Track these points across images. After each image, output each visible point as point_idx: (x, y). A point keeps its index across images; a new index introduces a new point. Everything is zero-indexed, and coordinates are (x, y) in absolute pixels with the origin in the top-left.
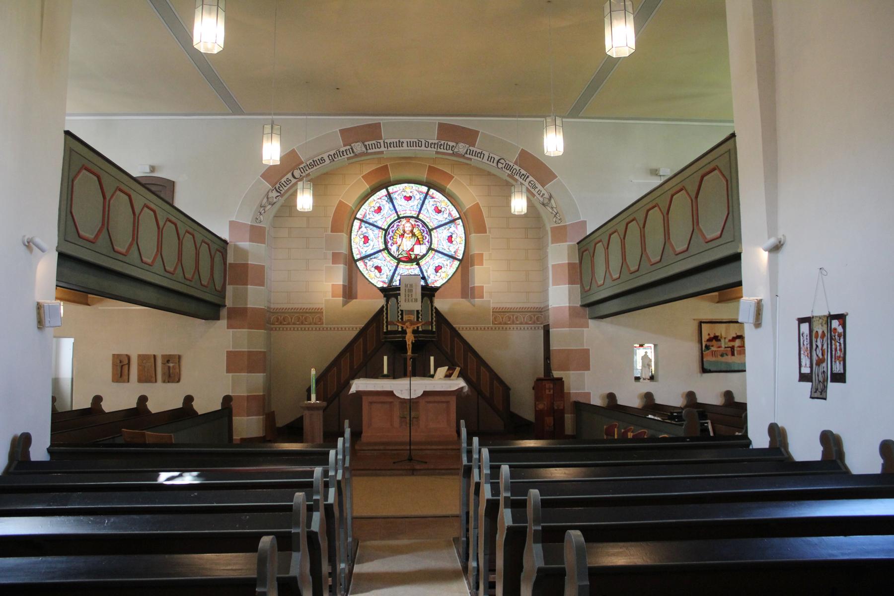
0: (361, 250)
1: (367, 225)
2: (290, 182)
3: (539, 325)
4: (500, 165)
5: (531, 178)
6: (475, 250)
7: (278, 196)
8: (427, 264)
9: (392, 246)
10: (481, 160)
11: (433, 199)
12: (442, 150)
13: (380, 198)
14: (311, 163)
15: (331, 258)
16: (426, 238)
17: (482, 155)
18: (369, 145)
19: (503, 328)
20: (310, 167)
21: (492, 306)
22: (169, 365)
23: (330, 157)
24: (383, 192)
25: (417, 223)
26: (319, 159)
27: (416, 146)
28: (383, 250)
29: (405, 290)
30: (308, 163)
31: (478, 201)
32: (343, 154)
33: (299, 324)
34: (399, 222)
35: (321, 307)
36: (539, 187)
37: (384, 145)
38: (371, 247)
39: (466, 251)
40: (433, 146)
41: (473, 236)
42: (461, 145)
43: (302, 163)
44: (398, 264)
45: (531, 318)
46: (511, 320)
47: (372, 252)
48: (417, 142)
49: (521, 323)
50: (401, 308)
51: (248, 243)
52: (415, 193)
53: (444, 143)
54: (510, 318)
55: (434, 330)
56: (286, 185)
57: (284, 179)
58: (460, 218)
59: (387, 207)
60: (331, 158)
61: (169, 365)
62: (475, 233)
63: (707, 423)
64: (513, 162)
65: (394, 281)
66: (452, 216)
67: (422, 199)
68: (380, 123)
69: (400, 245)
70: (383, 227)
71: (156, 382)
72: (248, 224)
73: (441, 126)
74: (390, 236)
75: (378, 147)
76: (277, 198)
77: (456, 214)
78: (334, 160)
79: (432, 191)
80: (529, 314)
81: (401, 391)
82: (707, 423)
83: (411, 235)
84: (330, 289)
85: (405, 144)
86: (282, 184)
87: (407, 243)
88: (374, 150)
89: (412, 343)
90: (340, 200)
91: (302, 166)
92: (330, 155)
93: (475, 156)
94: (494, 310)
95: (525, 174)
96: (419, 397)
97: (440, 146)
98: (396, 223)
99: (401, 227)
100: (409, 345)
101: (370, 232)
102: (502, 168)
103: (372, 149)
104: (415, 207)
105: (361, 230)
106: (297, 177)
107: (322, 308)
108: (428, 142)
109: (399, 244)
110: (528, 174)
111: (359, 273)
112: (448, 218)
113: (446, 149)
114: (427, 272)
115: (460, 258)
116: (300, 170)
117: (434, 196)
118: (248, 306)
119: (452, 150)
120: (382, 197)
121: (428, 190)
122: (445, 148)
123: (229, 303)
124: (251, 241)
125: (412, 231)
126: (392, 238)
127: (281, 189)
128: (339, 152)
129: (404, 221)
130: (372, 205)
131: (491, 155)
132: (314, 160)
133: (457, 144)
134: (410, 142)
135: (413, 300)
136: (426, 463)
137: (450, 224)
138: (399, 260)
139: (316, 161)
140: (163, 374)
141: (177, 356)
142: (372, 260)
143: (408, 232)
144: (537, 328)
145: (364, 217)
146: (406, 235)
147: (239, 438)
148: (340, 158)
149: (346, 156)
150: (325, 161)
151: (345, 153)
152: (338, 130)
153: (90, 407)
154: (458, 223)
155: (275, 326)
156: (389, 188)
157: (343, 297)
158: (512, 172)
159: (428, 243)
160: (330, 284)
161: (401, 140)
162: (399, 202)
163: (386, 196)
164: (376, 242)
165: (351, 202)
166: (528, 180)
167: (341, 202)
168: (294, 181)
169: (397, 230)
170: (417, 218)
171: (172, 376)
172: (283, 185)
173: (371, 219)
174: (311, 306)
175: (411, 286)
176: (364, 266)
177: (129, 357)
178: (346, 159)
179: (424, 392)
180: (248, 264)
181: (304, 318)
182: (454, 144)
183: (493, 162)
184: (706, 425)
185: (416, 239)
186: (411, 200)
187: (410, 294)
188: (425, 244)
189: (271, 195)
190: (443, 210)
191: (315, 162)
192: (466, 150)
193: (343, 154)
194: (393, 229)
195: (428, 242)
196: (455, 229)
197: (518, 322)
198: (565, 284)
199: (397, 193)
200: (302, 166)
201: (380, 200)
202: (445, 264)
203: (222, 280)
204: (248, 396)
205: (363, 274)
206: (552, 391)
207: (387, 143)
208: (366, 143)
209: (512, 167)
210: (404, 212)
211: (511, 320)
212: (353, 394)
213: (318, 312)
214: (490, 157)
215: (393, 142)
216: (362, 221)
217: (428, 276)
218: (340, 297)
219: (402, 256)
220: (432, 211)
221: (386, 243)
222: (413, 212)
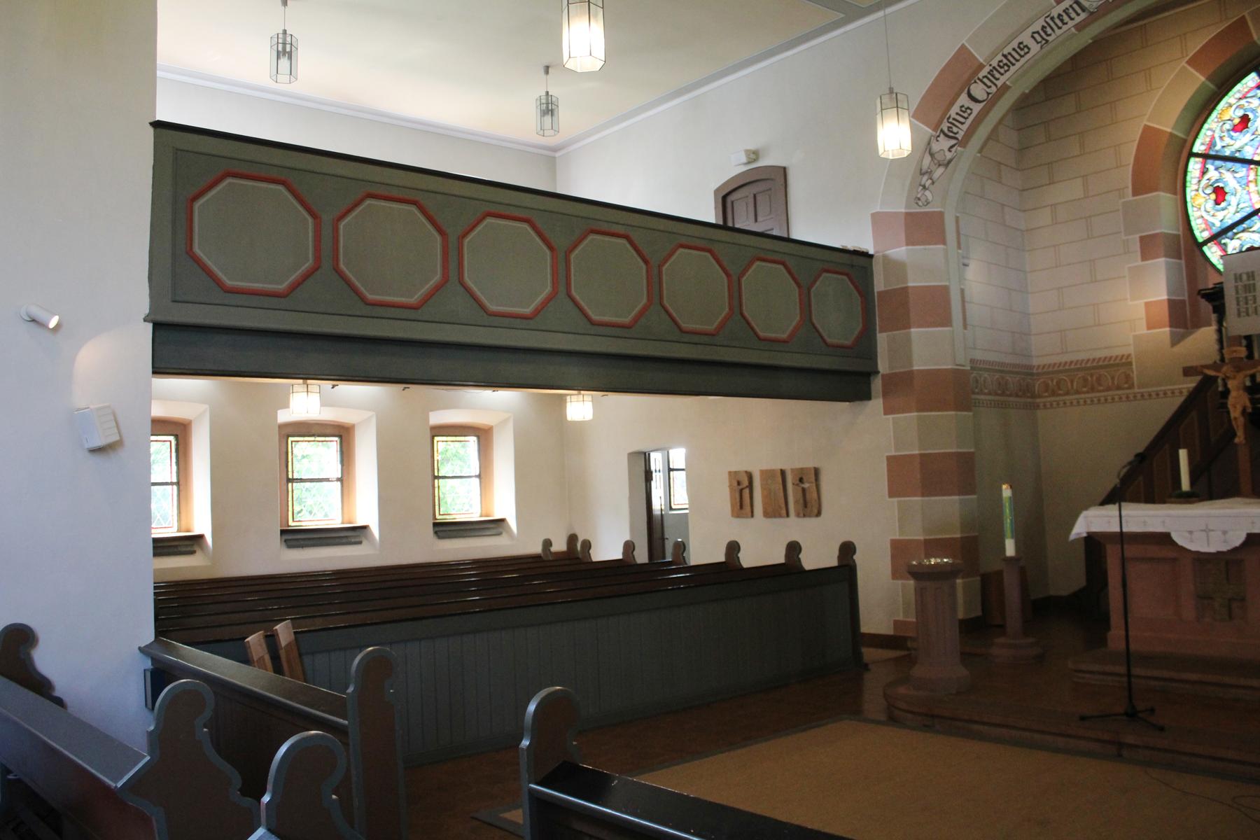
1: (1218, 163)
2: (969, 111)
14: (1001, 61)
15: (1139, 249)
20: (1002, 71)
22: (803, 485)
26: (1014, 49)
29: (1236, 287)
30: (995, 63)
32: (1062, 21)
33: (1088, 392)
35: (1126, 353)
38: (1232, 209)
43: (981, 67)
47: (1238, 217)
51: (904, 248)
56: (962, 120)
57: (955, 109)
60: (1039, 39)
61: (803, 485)
71: (788, 515)
72: (902, 212)
76: (953, 149)
78: (1047, 41)
81: (1191, 532)
84: (1141, 313)
86: (954, 119)
89: (1244, 412)
92: (1034, 33)
101: (1228, 176)
105: (1206, 177)
106: (980, 99)
107: (1129, 356)
116: (981, 81)
120: (1248, 92)
123: (883, 366)
124: (909, 242)
127: (955, 130)
128: (1052, 19)
132: (1005, 52)
136: (1162, 729)
139: (1010, 54)
145: (1210, 148)
148: (1058, 32)
149: (1071, 23)
150: (1029, 49)
151: (1066, 18)
153: (620, 557)
160: (1141, 303)
168: (977, 108)
171: (810, 506)
173: (1226, 149)
177: (750, 476)
178: (1073, 29)
181: (1055, 381)
187: (1250, 296)
189: (936, 147)
193: (1062, 21)
201: (1243, 102)
212: (1073, 541)
218: (1164, 327)
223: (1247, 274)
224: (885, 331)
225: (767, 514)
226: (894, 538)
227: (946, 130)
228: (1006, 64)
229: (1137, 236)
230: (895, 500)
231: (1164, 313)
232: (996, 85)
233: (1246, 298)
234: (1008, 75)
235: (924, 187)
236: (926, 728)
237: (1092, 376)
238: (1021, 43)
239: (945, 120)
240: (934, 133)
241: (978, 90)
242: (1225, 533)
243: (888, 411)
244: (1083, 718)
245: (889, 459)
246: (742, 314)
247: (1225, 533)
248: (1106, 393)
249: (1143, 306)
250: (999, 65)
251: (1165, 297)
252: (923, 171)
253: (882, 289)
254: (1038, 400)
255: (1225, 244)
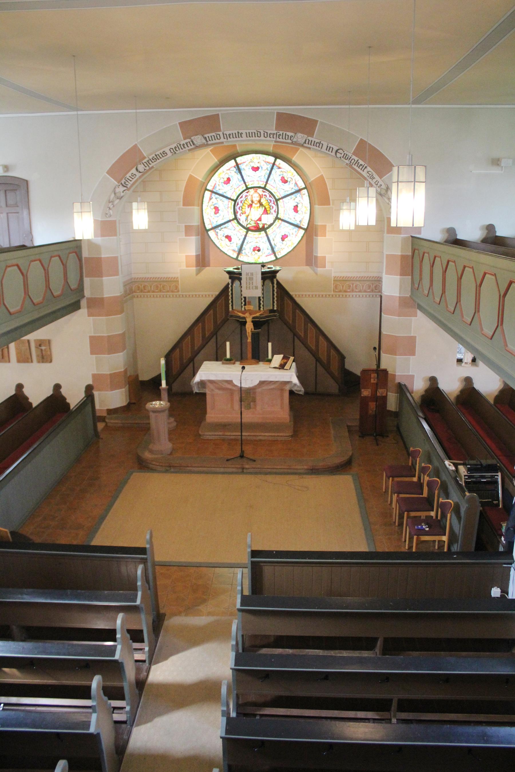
0: (212, 220)
1: (217, 196)
2: (135, 176)
3: (377, 293)
4: (338, 155)
5: (369, 169)
6: (319, 222)
7: (124, 191)
8: (274, 232)
9: (240, 215)
10: (319, 149)
11: (280, 170)
12: (281, 140)
13: (229, 169)
16: (273, 207)
17: (321, 145)
18: (208, 137)
19: (343, 296)
20: (153, 161)
21: (333, 275)
22: (41, 348)
23: (172, 150)
24: (232, 163)
25: (264, 194)
26: (161, 153)
27: (255, 137)
28: (233, 220)
29: (246, 278)
30: (151, 157)
31: (323, 173)
34: (247, 193)
36: (377, 178)
37: (224, 136)
39: (311, 220)
40: (272, 136)
41: (317, 207)
42: (299, 135)
43: (145, 158)
44: (247, 233)
45: (370, 287)
46: (351, 288)
48: (256, 132)
49: (360, 291)
50: (244, 295)
52: (263, 163)
53: (283, 134)
54: (350, 286)
55: (275, 309)
56: (131, 179)
57: (129, 174)
58: (305, 188)
59: (235, 177)
61: (41, 348)
62: (319, 205)
63: (498, 476)
64: (352, 153)
65: (243, 249)
66: (297, 186)
67: (269, 169)
68: (218, 115)
69: (248, 215)
70: (232, 198)
71: (32, 362)
72: (99, 220)
73: (280, 116)
74: (239, 206)
75: (218, 139)
76: (125, 192)
77: (302, 185)
78: (175, 153)
79: (279, 161)
80: (368, 283)
82: (498, 476)
83: (258, 205)
84: (184, 260)
85: (244, 135)
86: (128, 179)
87: (255, 213)
88: (214, 141)
90: (190, 175)
91: (145, 160)
93: (314, 145)
94: (336, 279)
95: (363, 165)
96: (255, 386)
97: (279, 136)
98: (244, 194)
99: (249, 197)
100: (249, 333)
102: (340, 157)
103: (212, 140)
104: (263, 177)
105: (212, 201)
106: (141, 171)
107: (178, 278)
108: (267, 133)
109: (247, 214)
110: (366, 165)
111: (211, 243)
112: (294, 188)
113: (285, 139)
114: (274, 241)
115: (305, 227)
116: (143, 164)
117: (280, 166)
118: (105, 296)
119: (291, 140)
121: (275, 160)
122: (284, 138)
123: (87, 293)
125: (259, 201)
126: (241, 209)
127: (127, 183)
128: (180, 145)
129: (252, 191)
130: (223, 175)
131: (329, 145)
132: (157, 154)
133: (296, 134)
134: (249, 133)
135: (254, 288)
136: (255, 461)
137: (296, 194)
138: (248, 229)
139: (158, 155)
140: (38, 356)
141: (47, 341)
142: (222, 230)
143: (256, 202)
144: (374, 296)
146: (254, 205)
147: (106, 408)
148: (181, 150)
149: (187, 148)
151: (186, 146)
152: (177, 123)
154: (304, 193)
155: (137, 294)
156: (237, 159)
157: (196, 267)
158: (351, 162)
159: (275, 212)
161: (240, 132)
162: (247, 172)
163: (235, 167)
164: (227, 213)
165: (200, 177)
166: (365, 170)
167: (191, 176)
168: (138, 175)
169: (246, 199)
170: (264, 188)
172: (129, 180)
174: (166, 276)
175: (252, 274)
176: (215, 236)
179: (260, 382)
180: (101, 258)
181: (161, 286)
182: (292, 134)
183: (332, 152)
184: (497, 477)
185: (264, 208)
186: (258, 170)
188: (272, 214)
189: (117, 190)
190: (289, 180)
191: (158, 156)
192: (304, 140)
194: (242, 199)
195: (275, 211)
196: (301, 199)
197: (357, 290)
198: (397, 275)
199: (245, 164)
200: (145, 160)
201: (228, 172)
202: (291, 233)
203: (79, 275)
204: (111, 375)
205: (214, 243)
206: (376, 380)
207: (226, 134)
208: (206, 136)
209: (351, 157)
210: (252, 183)
211: (351, 288)
213: (175, 281)
214: (329, 148)
215: (232, 134)
216: (212, 192)
217: (275, 244)
219: (251, 226)
220: (279, 181)
221: (235, 213)
222: (260, 182)
223: (251, 273)
224: (88, 277)
225: (19, 361)
226: (93, 373)
227: (123, 183)
228: (156, 159)
229: (184, 225)
230: (94, 356)
231: (194, 261)
232: (149, 166)
233: (250, 282)
234: (155, 163)
235: (110, 209)
236: (167, 471)
237: (160, 285)
238: (164, 151)
239: (124, 179)
240: (118, 184)
241: (141, 168)
242: (252, 380)
243: (90, 315)
244: (227, 460)
245: (91, 337)
246: (49, 288)
247: (252, 380)
248: (166, 293)
249: (185, 257)
250: (152, 159)
251: (194, 254)
252: (110, 201)
253: (87, 256)
254: (134, 294)
255: (217, 232)
